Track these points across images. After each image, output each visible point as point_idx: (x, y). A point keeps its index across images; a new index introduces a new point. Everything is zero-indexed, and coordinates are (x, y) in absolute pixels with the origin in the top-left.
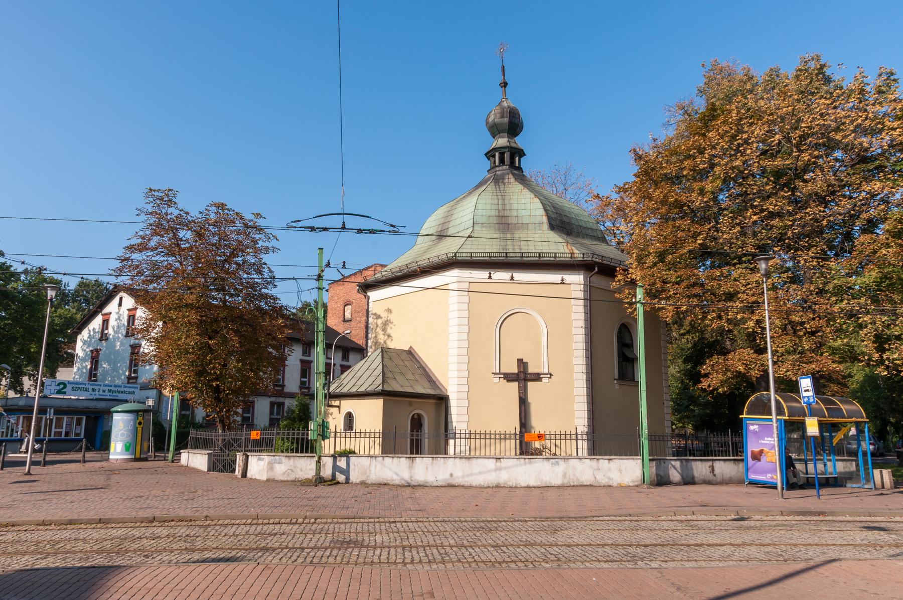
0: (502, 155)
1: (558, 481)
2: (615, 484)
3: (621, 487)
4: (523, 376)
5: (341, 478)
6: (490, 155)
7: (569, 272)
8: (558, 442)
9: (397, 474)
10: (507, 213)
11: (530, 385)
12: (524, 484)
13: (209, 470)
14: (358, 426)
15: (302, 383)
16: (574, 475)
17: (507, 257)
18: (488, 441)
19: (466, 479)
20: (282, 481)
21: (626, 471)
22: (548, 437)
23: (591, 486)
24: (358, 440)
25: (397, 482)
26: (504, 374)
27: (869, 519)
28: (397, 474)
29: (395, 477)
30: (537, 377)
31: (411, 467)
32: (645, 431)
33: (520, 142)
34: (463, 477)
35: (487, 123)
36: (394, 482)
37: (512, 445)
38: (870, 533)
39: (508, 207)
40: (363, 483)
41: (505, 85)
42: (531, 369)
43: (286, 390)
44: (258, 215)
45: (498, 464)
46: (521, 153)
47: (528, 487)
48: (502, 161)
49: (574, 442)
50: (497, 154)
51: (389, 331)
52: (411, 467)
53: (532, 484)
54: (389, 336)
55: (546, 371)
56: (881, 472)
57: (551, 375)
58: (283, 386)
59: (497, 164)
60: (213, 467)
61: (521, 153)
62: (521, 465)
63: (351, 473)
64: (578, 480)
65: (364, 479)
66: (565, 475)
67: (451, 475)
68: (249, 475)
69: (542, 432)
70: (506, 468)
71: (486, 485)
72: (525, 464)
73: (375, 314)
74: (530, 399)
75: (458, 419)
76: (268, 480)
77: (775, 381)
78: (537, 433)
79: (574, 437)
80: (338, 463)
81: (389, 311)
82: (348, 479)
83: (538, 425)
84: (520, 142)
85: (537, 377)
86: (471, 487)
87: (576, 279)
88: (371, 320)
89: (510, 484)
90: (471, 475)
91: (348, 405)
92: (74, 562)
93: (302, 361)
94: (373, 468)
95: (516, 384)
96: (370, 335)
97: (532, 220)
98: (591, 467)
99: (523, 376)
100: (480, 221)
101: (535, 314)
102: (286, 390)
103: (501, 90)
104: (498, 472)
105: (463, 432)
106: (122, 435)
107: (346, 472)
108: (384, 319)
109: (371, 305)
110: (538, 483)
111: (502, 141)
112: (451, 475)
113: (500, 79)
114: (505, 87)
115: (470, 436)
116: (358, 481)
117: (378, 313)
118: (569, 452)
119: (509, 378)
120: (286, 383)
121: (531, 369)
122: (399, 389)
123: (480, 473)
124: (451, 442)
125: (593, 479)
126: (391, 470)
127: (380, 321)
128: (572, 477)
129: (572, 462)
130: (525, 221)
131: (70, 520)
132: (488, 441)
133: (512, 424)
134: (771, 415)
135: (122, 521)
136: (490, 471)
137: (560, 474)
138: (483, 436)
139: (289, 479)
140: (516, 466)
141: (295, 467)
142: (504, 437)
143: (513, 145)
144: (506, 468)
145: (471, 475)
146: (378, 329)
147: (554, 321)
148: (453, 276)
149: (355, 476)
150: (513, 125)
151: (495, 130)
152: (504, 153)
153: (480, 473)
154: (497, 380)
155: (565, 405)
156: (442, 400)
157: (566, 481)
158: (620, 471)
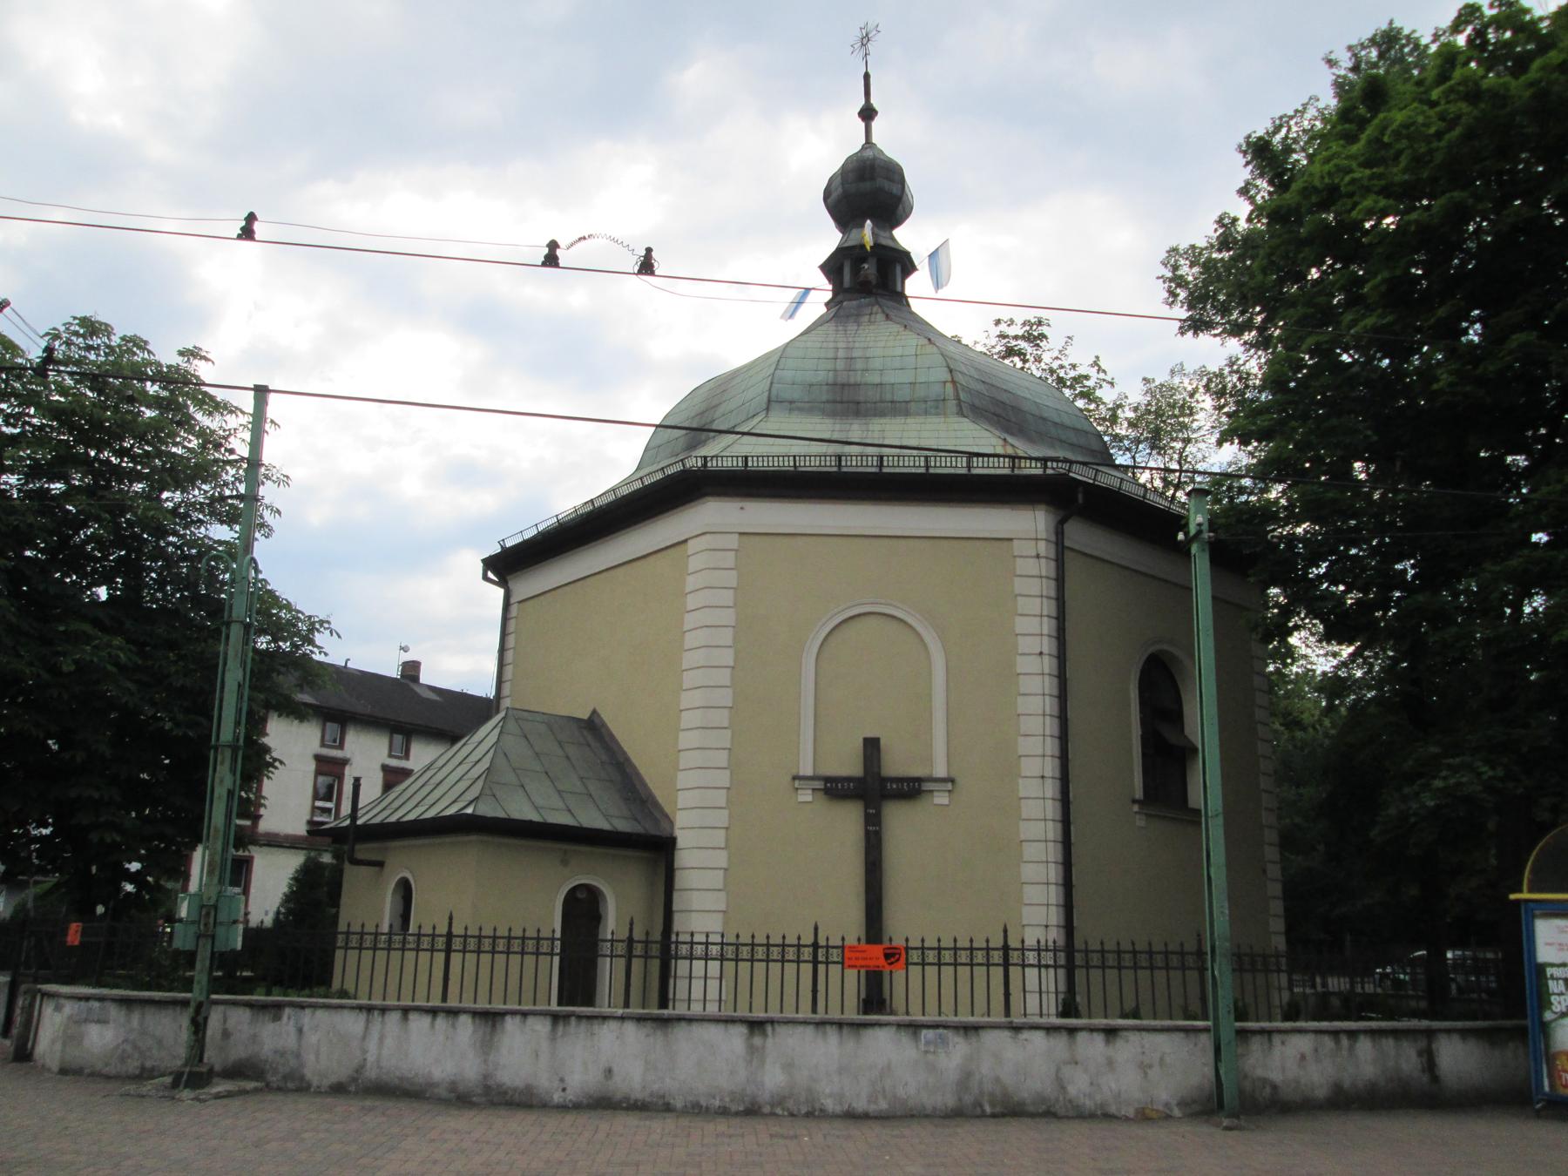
21: (1152, 1062)
22: (915, 956)
26: (827, 779)
30: (912, 789)
31: (487, 1046)
37: (844, 988)
39: (859, 365)
42: (896, 764)
43: (264, 826)
44: (192, 353)
52: (487, 1046)
57: (952, 781)
58: (256, 818)
64: (997, 1080)
75: (702, 910)
77: (865, 1013)
79: (457, 944)
83: (902, 926)
85: (912, 789)
92: (1226, 904)
99: (873, 789)
100: (787, 396)
102: (264, 826)
115: (733, 952)
119: (835, 789)
122: (528, 814)
129: (991, 1039)
130: (900, 395)
133: (843, 920)
134: (1530, 891)
143: (884, 242)
154: (806, 796)
156: (655, 849)
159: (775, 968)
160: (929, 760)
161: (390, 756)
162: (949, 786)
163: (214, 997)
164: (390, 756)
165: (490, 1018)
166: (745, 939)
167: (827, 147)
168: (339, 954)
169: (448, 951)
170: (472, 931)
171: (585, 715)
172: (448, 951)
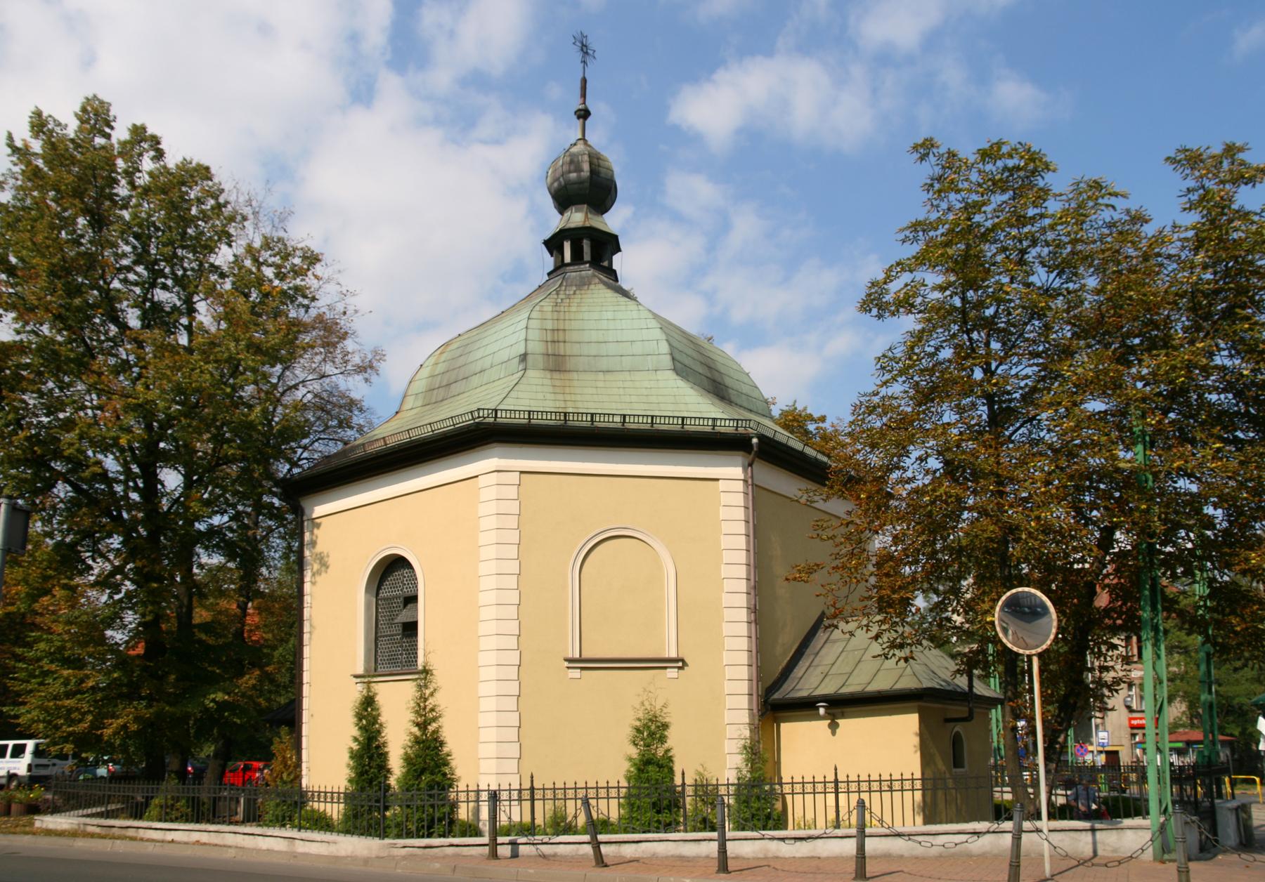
6: (553, 244)
7: (343, 490)
17: (714, 426)
24: (809, 798)
27: (170, 836)
33: (612, 221)
41: (584, 114)
48: (577, 257)
49: (831, 798)
50: (567, 247)
55: (673, 655)
56: (533, 818)
59: (568, 258)
84: (612, 221)
103: (579, 123)
111: (577, 218)
113: (577, 104)
118: (810, 816)
124: (1087, 825)
138: (809, 788)
148: (489, 469)
152: (580, 240)
162: (680, 664)
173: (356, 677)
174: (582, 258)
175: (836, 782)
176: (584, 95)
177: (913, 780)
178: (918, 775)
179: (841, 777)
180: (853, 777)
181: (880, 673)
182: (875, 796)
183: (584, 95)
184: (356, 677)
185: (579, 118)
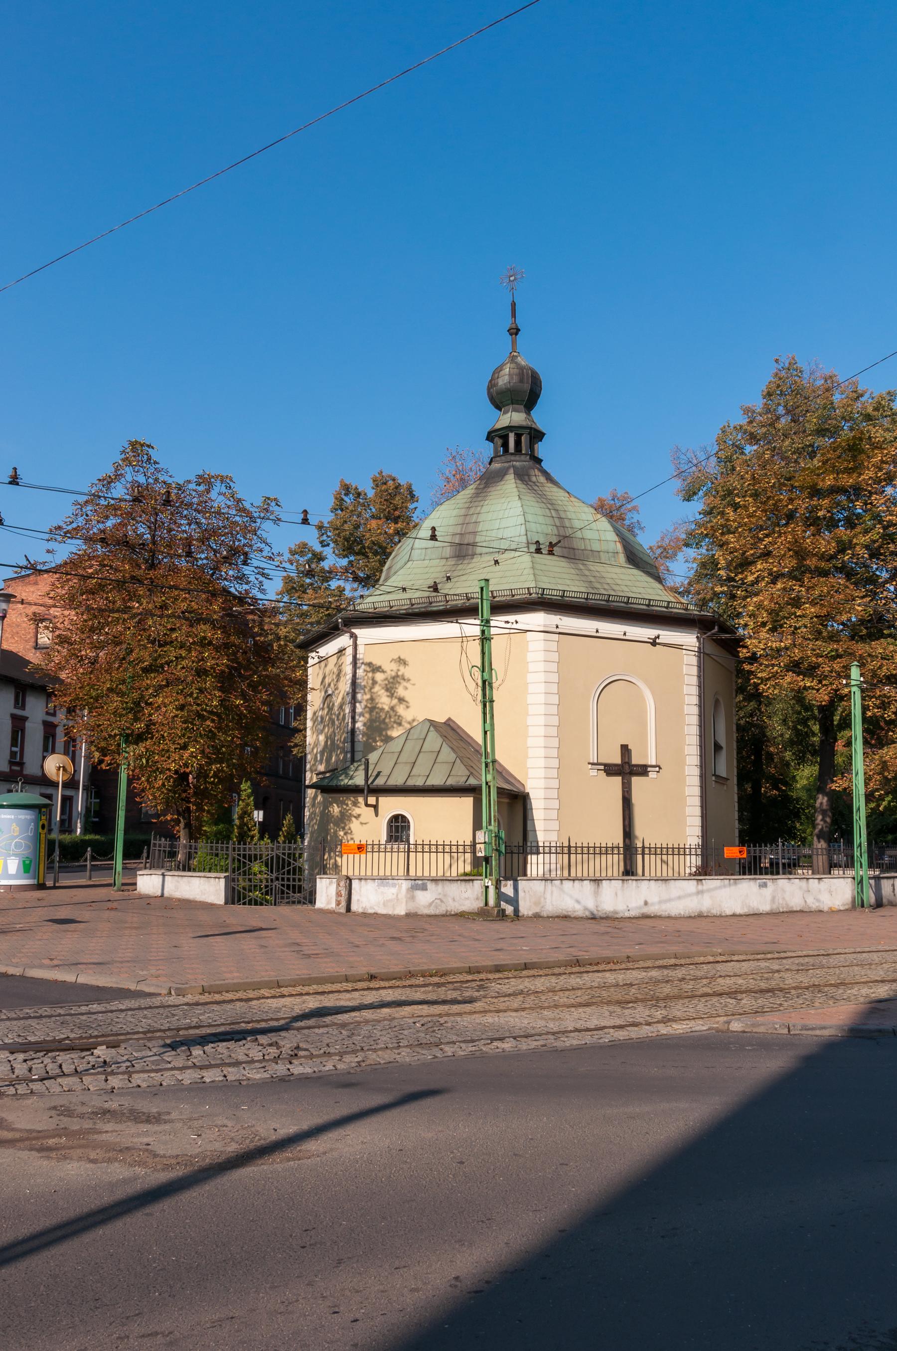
0: (518, 438)
1: (765, 907)
2: (826, 909)
3: (832, 912)
4: (626, 769)
5: (509, 909)
8: (664, 857)
9: (578, 902)
10: (569, 532)
11: (635, 779)
12: (729, 912)
13: (226, 903)
14: (415, 835)
15: (13, 754)
16: (784, 899)
18: (585, 856)
19: (664, 907)
20: (429, 916)
22: (369, 848)
23: (801, 911)
25: (580, 913)
26: (605, 765)
28: (578, 902)
29: (578, 907)
30: (643, 771)
31: (596, 894)
32: (97, 837)
33: (540, 417)
34: (660, 902)
35: (492, 384)
36: (576, 914)
37: (615, 862)
38: (443, 997)
40: (537, 916)
41: (515, 331)
45: (700, 887)
46: (537, 435)
47: (734, 915)
49: (566, 856)
51: (400, 691)
52: (596, 894)
53: (739, 911)
54: (401, 700)
55: (654, 763)
60: (234, 896)
61: (537, 435)
62: (725, 886)
63: (521, 903)
64: (586, 909)
65: (537, 910)
66: (773, 899)
67: (646, 903)
68: (354, 907)
69: (363, 842)
70: (709, 890)
71: (687, 915)
72: (730, 885)
73: (369, 664)
74: (635, 800)
76: (408, 915)
78: (357, 842)
79: (647, 851)
80: (503, 890)
81: (402, 661)
82: (516, 911)
83: (644, 833)
84: (540, 417)
85: (643, 771)
86: (669, 917)
87: (689, 639)
88: (360, 672)
89: (715, 912)
90: (670, 900)
91: (391, 806)
93: (14, 717)
94: (548, 896)
95: (619, 779)
96: (359, 696)
97: (604, 547)
98: (800, 888)
99: (626, 769)
101: (639, 683)
104: (700, 896)
105: (547, 844)
106: (17, 845)
107: (514, 901)
108: (390, 674)
109: (361, 649)
110: (744, 911)
111: (514, 417)
112: (646, 903)
113: (508, 323)
114: (516, 334)
116: (530, 913)
117: (377, 662)
119: (610, 770)
120: (25, 760)
121: (635, 760)
123: (679, 898)
125: (803, 903)
126: (571, 897)
127: (379, 677)
128: (781, 901)
131: (496, 966)
132: (585, 856)
135: (548, 966)
136: (690, 895)
137: (769, 898)
138: (426, 848)
139: (437, 912)
140: (720, 887)
141: (445, 895)
142: (606, 851)
144: (709, 890)
145: (670, 900)
146: (377, 688)
147: (661, 692)
149: (526, 907)
150: (526, 392)
151: (500, 399)
153: (679, 898)
155: (676, 808)
157: (775, 907)
158: (830, 892)
159: (433, 855)
160: (646, 756)
161: (15, 707)
162: (657, 769)
163: (640, 871)
164: (15, 707)
165: (597, 881)
166: (461, 843)
167: (495, 361)
168: (639, 857)
169: (569, 853)
170: (579, 845)
171: (442, 719)
172: (569, 853)
173: (593, 764)
174: (521, 451)
175: (569, 847)
176: (514, 315)
177: (373, 845)
178: (621, 845)
179: (647, 845)
180: (579, 845)
181: (421, 755)
182: (670, 857)
183: (514, 315)
184: (593, 764)
185: (511, 334)
